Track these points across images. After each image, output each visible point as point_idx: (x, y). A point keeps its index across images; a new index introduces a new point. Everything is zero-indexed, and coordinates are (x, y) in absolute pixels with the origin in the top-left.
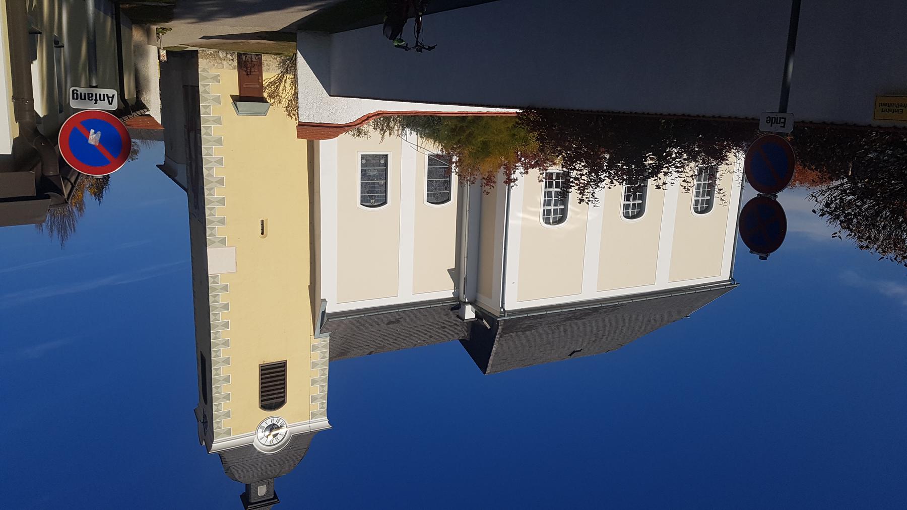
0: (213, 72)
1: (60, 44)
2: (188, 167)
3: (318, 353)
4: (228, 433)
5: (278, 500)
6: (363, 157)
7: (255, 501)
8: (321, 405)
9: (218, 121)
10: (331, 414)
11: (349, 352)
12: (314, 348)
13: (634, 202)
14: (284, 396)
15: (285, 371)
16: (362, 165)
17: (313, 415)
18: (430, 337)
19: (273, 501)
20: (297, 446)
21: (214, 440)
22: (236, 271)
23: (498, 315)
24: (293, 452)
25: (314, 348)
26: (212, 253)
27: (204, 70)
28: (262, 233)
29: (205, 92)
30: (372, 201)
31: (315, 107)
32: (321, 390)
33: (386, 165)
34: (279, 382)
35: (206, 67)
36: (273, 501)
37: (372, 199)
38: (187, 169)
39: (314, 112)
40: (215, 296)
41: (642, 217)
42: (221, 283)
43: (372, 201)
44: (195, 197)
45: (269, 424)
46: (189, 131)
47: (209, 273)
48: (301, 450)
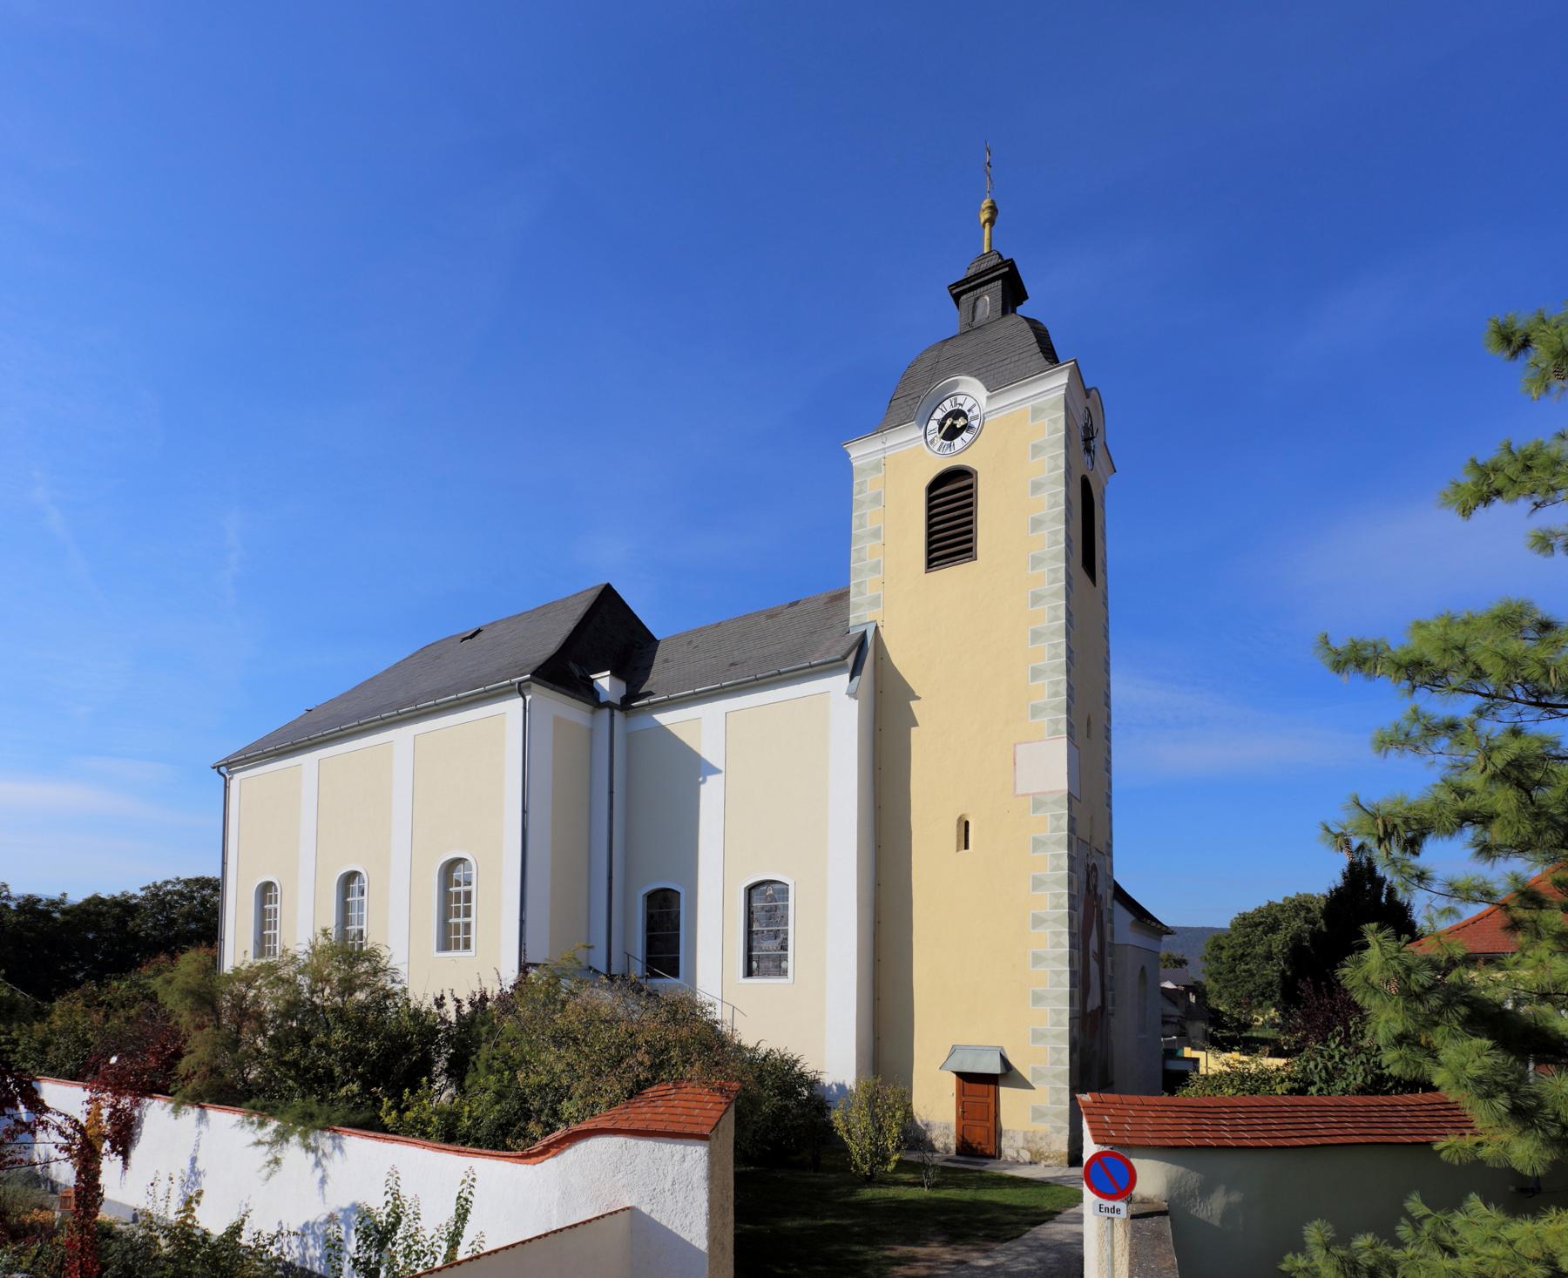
0: (1043, 1127)
1: (1369, 653)
2: (1108, 939)
3: (870, 593)
4: (1036, 412)
5: (950, 291)
6: (784, 973)
7: (992, 285)
8: (865, 487)
9: (1038, 1036)
10: (844, 472)
11: (826, 603)
12: (875, 602)
13: (458, 889)
14: (930, 500)
15: (929, 552)
16: (785, 958)
17: (877, 467)
18: (690, 643)
19: (961, 288)
20: (910, 402)
21: (1063, 392)
22: (1015, 745)
23: (535, 687)
24: (916, 390)
25: (875, 602)
26: (1058, 780)
27: (1058, 1131)
28: (967, 823)
29: (1057, 1091)
30: (771, 892)
31: (670, 1180)
32: (865, 518)
33: (749, 959)
34: (941, 526)
35: (1054, 1135)
36: (961, 288)
37: (770, 895)
38: (1112, 934)
39: (670, 1168)
40: (1056, 694)
41: (442, 862)
42: (1044, 721)
43: (771, 892)
44: (1095, 887)
45: (959, 439)
46: (1103, 1007)
47: (1066, 739)
48: (904, 394)
